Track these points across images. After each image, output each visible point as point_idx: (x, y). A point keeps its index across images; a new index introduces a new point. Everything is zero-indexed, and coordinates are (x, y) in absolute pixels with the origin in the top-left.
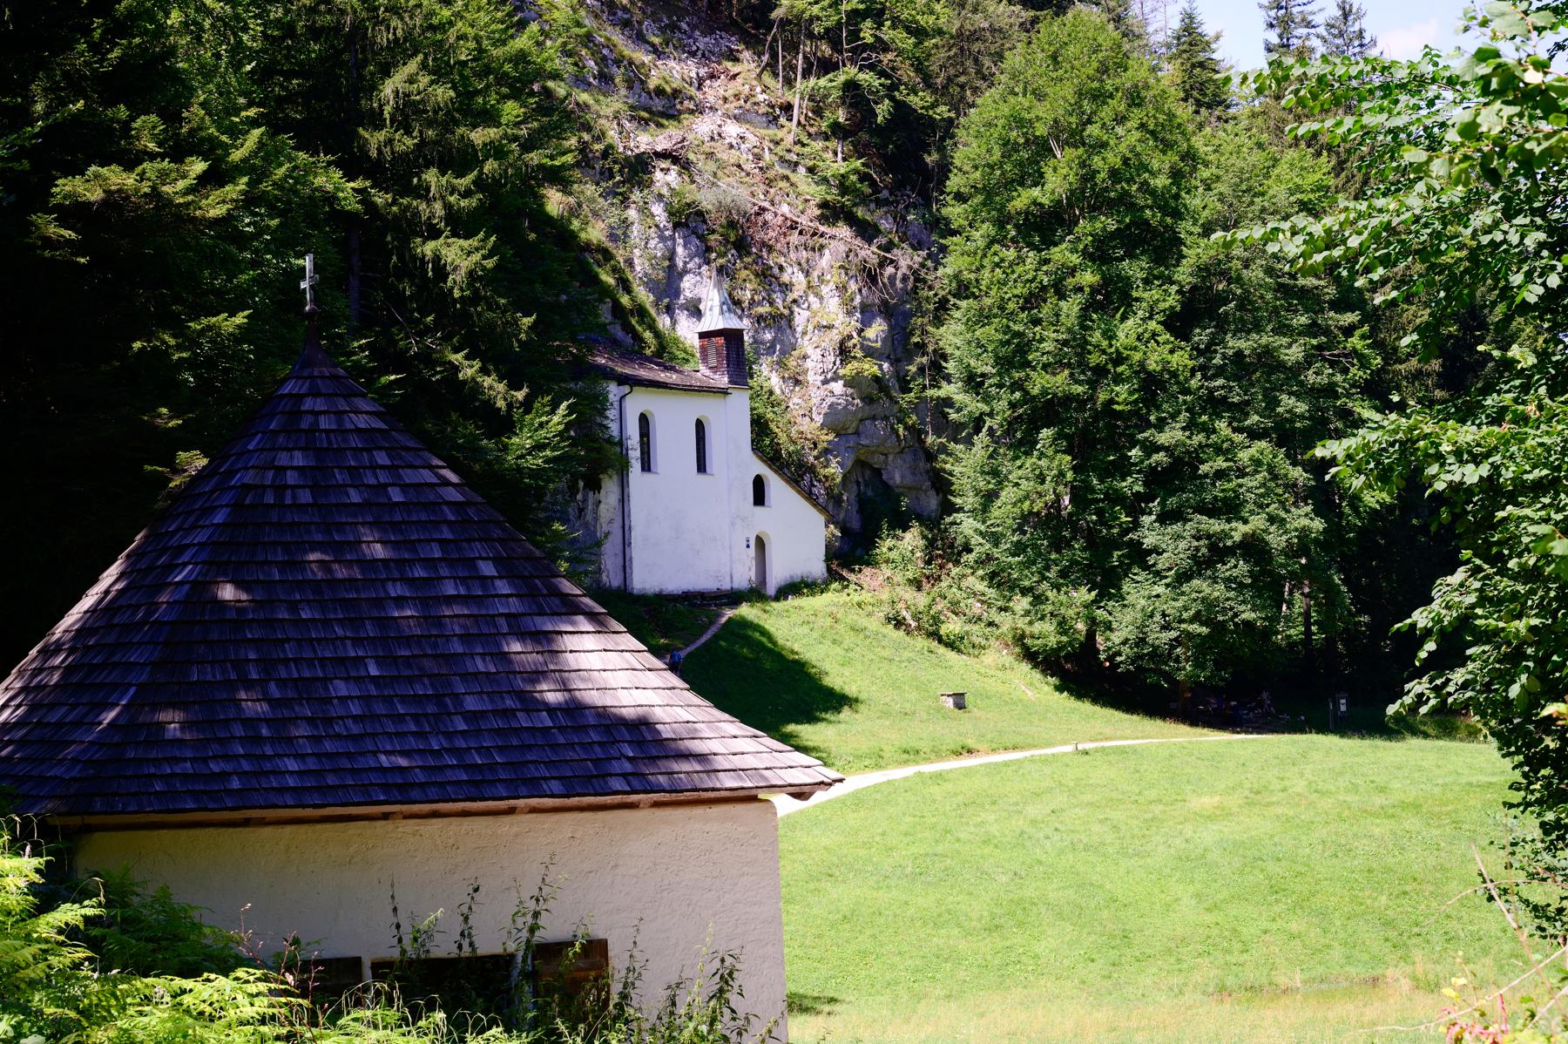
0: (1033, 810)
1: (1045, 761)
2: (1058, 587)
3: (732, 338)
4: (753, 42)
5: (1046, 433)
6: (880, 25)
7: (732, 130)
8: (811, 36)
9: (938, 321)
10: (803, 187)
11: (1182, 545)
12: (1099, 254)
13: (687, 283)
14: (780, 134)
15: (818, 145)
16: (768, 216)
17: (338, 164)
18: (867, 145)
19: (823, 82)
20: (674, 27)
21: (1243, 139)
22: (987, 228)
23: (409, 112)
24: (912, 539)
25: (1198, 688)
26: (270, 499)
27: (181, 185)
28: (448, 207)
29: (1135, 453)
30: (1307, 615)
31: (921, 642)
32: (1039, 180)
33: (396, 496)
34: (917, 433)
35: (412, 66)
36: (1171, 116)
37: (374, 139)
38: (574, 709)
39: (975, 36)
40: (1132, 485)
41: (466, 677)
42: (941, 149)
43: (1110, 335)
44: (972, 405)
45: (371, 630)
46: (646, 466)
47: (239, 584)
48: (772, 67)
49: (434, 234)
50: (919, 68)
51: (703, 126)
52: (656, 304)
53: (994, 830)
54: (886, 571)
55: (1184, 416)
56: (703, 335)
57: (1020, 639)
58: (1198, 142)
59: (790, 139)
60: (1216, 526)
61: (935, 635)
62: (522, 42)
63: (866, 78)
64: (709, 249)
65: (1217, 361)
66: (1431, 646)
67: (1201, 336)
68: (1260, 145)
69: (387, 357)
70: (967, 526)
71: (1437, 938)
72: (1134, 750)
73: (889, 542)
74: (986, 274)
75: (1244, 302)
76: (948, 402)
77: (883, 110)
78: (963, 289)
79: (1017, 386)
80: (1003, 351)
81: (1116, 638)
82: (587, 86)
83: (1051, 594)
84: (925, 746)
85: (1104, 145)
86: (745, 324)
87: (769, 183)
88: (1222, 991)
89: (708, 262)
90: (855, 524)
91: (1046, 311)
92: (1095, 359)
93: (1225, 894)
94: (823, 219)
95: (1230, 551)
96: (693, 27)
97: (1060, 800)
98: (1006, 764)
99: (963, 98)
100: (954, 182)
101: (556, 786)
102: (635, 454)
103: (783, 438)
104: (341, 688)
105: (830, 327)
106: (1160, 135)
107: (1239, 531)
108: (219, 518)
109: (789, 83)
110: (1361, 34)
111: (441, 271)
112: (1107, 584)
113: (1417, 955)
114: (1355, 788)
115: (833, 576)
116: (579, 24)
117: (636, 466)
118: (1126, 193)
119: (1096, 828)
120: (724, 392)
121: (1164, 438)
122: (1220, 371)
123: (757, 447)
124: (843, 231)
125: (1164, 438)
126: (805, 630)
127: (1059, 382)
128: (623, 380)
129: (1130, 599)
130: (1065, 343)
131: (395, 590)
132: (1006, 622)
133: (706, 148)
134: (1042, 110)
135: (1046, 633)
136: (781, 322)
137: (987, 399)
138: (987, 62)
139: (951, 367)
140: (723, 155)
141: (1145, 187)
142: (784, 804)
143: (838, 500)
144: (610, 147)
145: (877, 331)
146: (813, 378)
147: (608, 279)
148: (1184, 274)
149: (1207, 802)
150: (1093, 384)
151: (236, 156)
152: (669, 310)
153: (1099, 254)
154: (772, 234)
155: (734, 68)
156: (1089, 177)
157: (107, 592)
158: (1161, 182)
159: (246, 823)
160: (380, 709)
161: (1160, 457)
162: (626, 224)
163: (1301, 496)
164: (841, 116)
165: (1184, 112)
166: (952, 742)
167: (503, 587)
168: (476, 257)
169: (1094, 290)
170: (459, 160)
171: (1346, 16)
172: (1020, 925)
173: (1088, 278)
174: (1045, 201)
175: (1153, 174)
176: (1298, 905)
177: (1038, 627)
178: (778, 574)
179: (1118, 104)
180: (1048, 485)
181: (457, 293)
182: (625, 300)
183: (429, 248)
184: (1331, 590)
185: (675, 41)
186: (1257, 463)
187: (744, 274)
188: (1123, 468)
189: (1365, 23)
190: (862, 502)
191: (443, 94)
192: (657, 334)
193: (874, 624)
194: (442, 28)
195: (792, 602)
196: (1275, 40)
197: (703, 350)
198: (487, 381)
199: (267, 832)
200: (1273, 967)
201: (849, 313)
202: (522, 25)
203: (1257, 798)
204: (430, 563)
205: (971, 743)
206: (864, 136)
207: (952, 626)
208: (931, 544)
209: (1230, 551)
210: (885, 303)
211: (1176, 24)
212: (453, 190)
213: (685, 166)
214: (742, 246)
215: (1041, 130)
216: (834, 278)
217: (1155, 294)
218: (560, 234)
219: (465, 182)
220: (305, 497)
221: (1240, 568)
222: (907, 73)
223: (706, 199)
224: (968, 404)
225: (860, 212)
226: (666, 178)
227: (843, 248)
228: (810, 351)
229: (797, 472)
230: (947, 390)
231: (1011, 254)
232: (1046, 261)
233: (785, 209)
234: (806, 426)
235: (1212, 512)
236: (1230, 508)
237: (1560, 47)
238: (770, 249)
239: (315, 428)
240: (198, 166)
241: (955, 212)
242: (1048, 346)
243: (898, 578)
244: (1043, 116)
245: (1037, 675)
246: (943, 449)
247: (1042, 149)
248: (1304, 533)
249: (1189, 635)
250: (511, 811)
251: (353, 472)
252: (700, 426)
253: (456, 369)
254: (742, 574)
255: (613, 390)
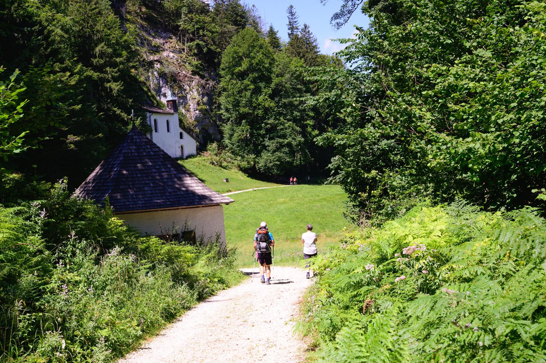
0: (245, 203)
1: (247, 192)
2: (247, 155)
3: (174, 102)
4: (175, 35)
5: (244, 121)
6: (204, 31)
7: (171, 55)
8: (188, 33)
9: (219, 97)
10: (188, 67)
11: (274, 145)
12: (254, 81)
13: (163, 89)
14: (182, 55)
15: (191, 58)
16: (180, 74)
17: (92, 69)
18: (201, 57)
19: (191, 44)
20: (157, 31)
21: (284, 55)
22: (229, 76)
23: (102, 55)
24: (215, 145)
25: (278, 175)
26: (130, 155)
27: (65, 78)
28: (112, 75)
29: (263, 125)
30: (300, 159)
31: (218, 168)
32: (241, 66)
33: (152, 153)
34: (215, 122)
35: (103, 44)
36: (269, 51)
37: (95, 61)
38: (187, 191)
39: (225, 33)
40: (263, 132)
41: (168, 186)
42: (218, 58)
43: (257, 100)
44: (227, 115)
45: (150, 178)
46: (156, 131)
47: (127, 170)
48: (180, 40)
49: (109, 81)
50: (213, 40)
51: (165, 54)
52: (156, 94)
53: (237, 207)
54: (209, 152)
55: (274, 117)
56: (168, 101)
57: (239, 166)
58: (275, 56)
59: (184, 56)
60: (281, 140)
61: (221, 166)
62: (125, 38)
63: (201, 42)
64: (168, 82)
65: (280, 104)
66: (333, 171)
67: (277, 99)
68: (288, 57)
69: (100, 109)
70: (227, 141)
71: (331, 226)
72: (265, 189)
73: (210, 146)
74: (230, 86)
75: (286, 92)
76: (222, 114)
77: (205, 50)
78: (224, 90)
79: (236, 111)
80: (234, 103)
81: (260, 165)
82: (138, 45)
83: (246, 156)
84: (220, 190)
85: (255, 58)
86: (176, 98)
87: (180, 66)
88: (287, 240)
89: (167, 85)
90: (202, 142)
91: (243, 94)
92: (254, 105)
93: (287, 219)
94: (192, 74)
95: (284, 146)
96: (161, 31)
97: (251, 201)
98: (238, 194)
99: (223, 47)
100: (222, 66)
101: (186, 204)
102: (153, 128)
103: (186, 124)
104: (146, 188)
105: (195, 99)
106: (267, 55)
107: (286, 141)
108: (121, 158)
109: (184, 44)
110: (309, 32)
111: (111, 90)
112: (258, 153)
113: (327, 230)
114: (312, 196)
115: (198, 154)
116: (136, 31)
117: (154, 131)
118: (260, 68)
119: (259, 206)
120: (173, 114)
121: (269, 122)
122: (281, 107)
123: (180, 126)
124: (197, 77)
125: (269, 122)
126: (193, 166)
127: (246, 110)
128: (150, 112)
129: (263, 157)
130: (247, 101)
131: (154, 170)
132: (236, 162)
133: (166, 59)
134: (240, 50)
135: (244, 164)
136: (184, 98)
137: (231, 114)
138: (228, 39)
139: (222, 106)
140: (170, 61)
141: (263, 67)
142: (224, 205)
143: (198, 137)
144: (144, 59)
145: (205, 99)
146: (192, 110)
147: (145, 89)
148: (273, 85)
149: (282, 200)
150: (254, 110)
151: (76, 71)
152: (159, 96)
153: (254, 81)
154: (181, 78)
155: (171, 41)
156: (251, 64)
157: (98, 172)
158: (267, 65)
159: (133, 213)
160: (154, 192)
161: (269, 126)
162: (149, 77)
163: (300, 133)
164: (196, 51)
165: (271, 50)
166: (226, 189)
167: (172, 169)
168: (119, 87)
169: (253, 89)
170: (114, 65)
171: (306, 27)
172: (244, 228)
173: (252, 87)
174: (242, 70)
175: (265, 64)
176: (302, 221)
177: (243, 163)
178: (186, 153)
179: (257, 48)
180: (245, 132)
181: (115, 95)
182: (149, 94)
183: (108, 85)
184: (306, 153)
185: (157, 35)
186: (289, 126)
187: (175, 87)
188: (260, 128)
189: (309, 29)
190: (203, 137)
191: (110, 50)
192: (157, 101)
193: (207, 164)
194: (109, 35)
195: (189, 160)
196: (290, 32)
197: (168, 105)
198: (122, 114)
199: (136, 214)
200: (297, 234)
201: (199, 95)
202: (125, 33)
203: (292, 199)
204: (159, 165)
205: (230, 189)
206: (201, 56)
207: (224, 164)
208: (219, 146)
209: (284, 146)
210: (207, 93)
211: (268, 29)
212: (113, 72)
213: (161, 63)
214: (175, 81)
215: (240, 54)
216: (196, 88)
217: (267, 90)
218: (134, 79)
219: (115, 70)
220: (136, 154)
221: (286, 149)
222: (210, 41)
223: (167, 71)
224: (226, 115)
225: (201, 73)
226: (157, 66)
227: (197, 81)
228: (191, 104)
229: (189, 131)
230: (221, 112)
231: (235, 82)
232: (243, 83)
233: (184, 72)
234: (190, 121)
235: (280, 137)
236: (284, 136)
237: (384, 361)
238: (181, 81)
239: (136, 142)
240: (68, 74)
241: (222, 73)
242: (243, 102)
243: (212, 154)
244: (241, 51)
245: (243, 174)
246: (221, 125)
247: (241, 58)
248: (300, 141)
249: (276, 164)
250: (178, 209)
251: (144, 149)
252: (168, 122)
253: (115, 111)
254: (179, 154)
255: (148, 114)
